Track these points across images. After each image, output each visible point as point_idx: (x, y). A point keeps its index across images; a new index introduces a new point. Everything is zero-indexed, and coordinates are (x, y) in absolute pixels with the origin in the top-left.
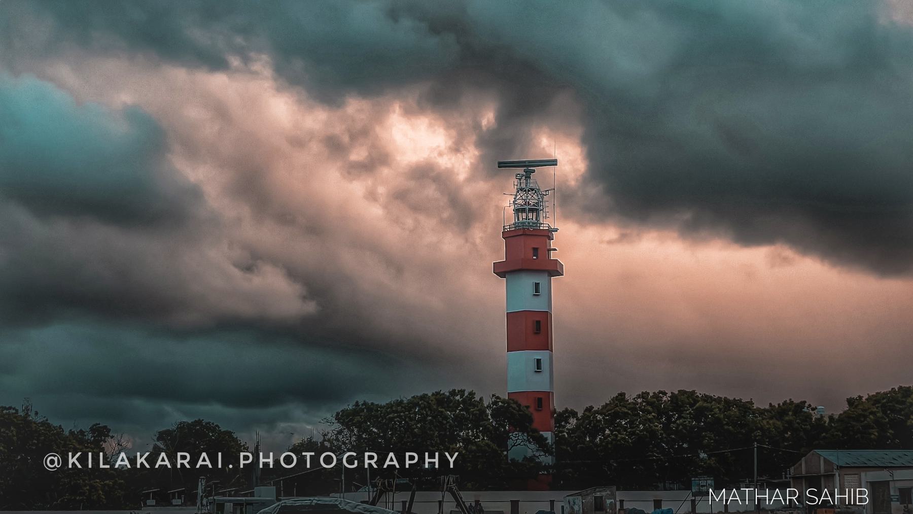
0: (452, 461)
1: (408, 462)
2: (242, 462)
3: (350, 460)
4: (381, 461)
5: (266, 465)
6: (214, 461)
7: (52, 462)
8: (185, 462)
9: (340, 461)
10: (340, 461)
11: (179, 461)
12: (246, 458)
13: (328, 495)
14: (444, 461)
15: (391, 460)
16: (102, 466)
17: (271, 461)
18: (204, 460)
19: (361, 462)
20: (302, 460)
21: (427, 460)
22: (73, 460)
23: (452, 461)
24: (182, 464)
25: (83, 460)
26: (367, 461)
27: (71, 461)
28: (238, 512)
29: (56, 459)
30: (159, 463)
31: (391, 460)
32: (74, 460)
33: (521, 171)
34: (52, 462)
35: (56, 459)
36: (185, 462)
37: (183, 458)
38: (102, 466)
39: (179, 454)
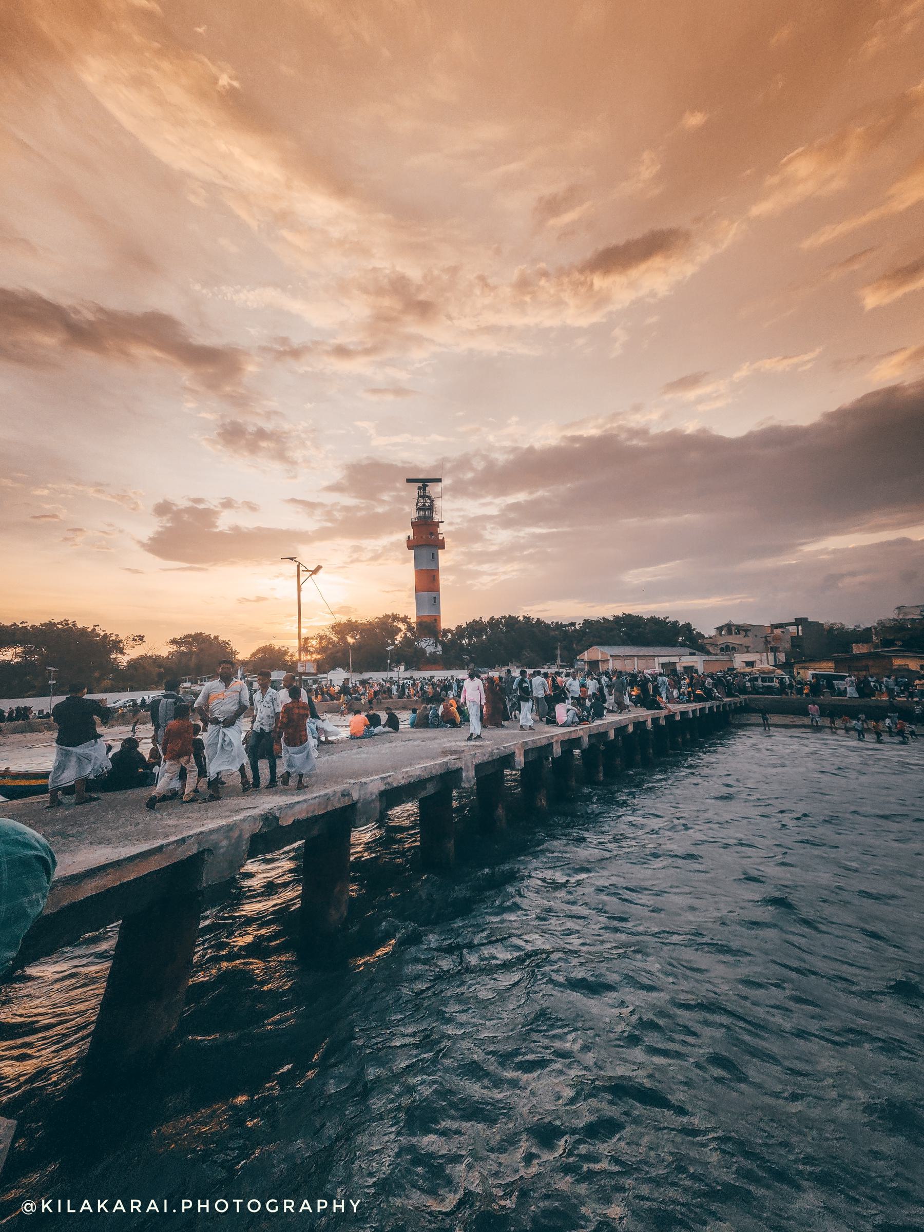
0: (355, 1206)
1: (319, 1208)
2: (184, 1208)
3: (272, 1206)
4: (144, 1207)
5: (339, 1209)
6: (161, 1207)
7: (28, 1207)
8: (137, 1207)
9: (263, 1205)
10: (263, 1205)
11: (132, 1207)
12: (322, 1204)
13: (834, 552)
14: (348, 1206)
15: (306, 1206)
16: (69, 1211)
17: (342, 1206)
18: (119, 1206)
19: (281, 1208)
20: (233, 1205)
21: (200, 1206)
22: (45, 1206)
23: (355, 1206)
24: (135, 1209)
25: (54, 1206)
26: (286, 1207)
27: (99, 1207)
28: (922, 1103)
29: (31, 1205)
30: (116, 1208)
31: (86, 1206)
32: (103, 1205)
33: (421, 485)
34: (28, 1207)
35: (31, 1205)
36: (137, 1207)
37: (136, 1204)
38: (69, 1211)
39: (132, 1201)
